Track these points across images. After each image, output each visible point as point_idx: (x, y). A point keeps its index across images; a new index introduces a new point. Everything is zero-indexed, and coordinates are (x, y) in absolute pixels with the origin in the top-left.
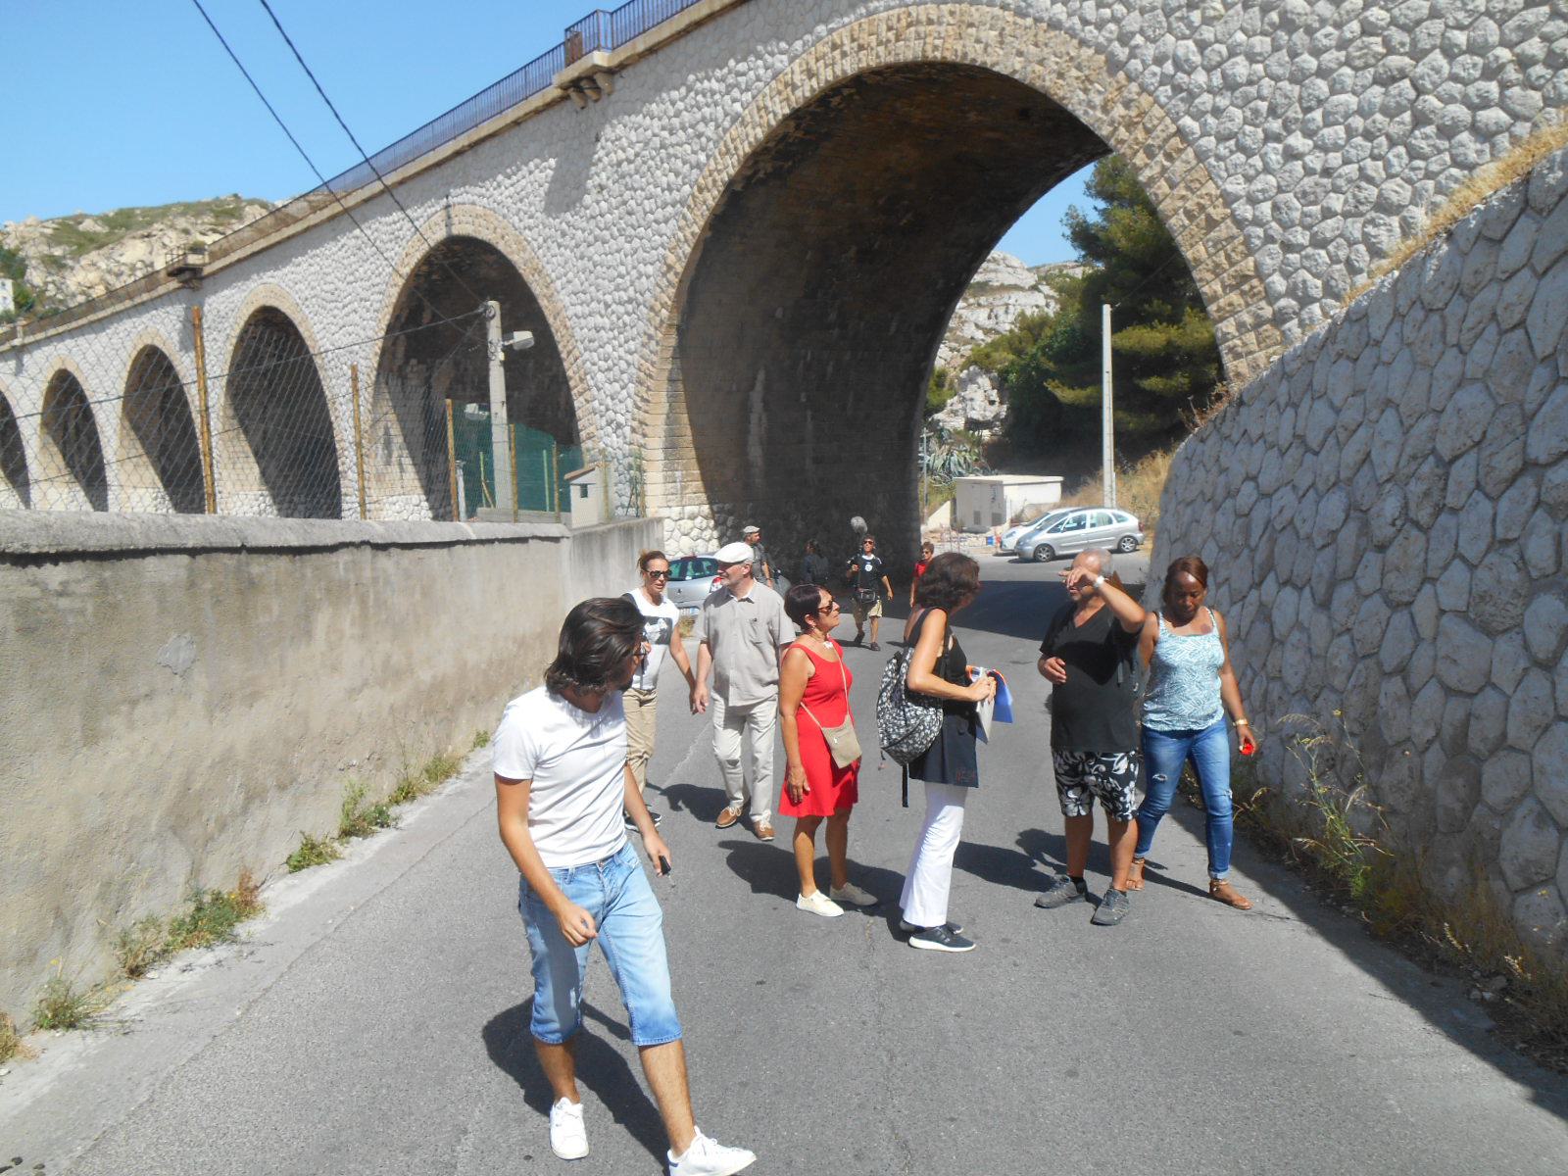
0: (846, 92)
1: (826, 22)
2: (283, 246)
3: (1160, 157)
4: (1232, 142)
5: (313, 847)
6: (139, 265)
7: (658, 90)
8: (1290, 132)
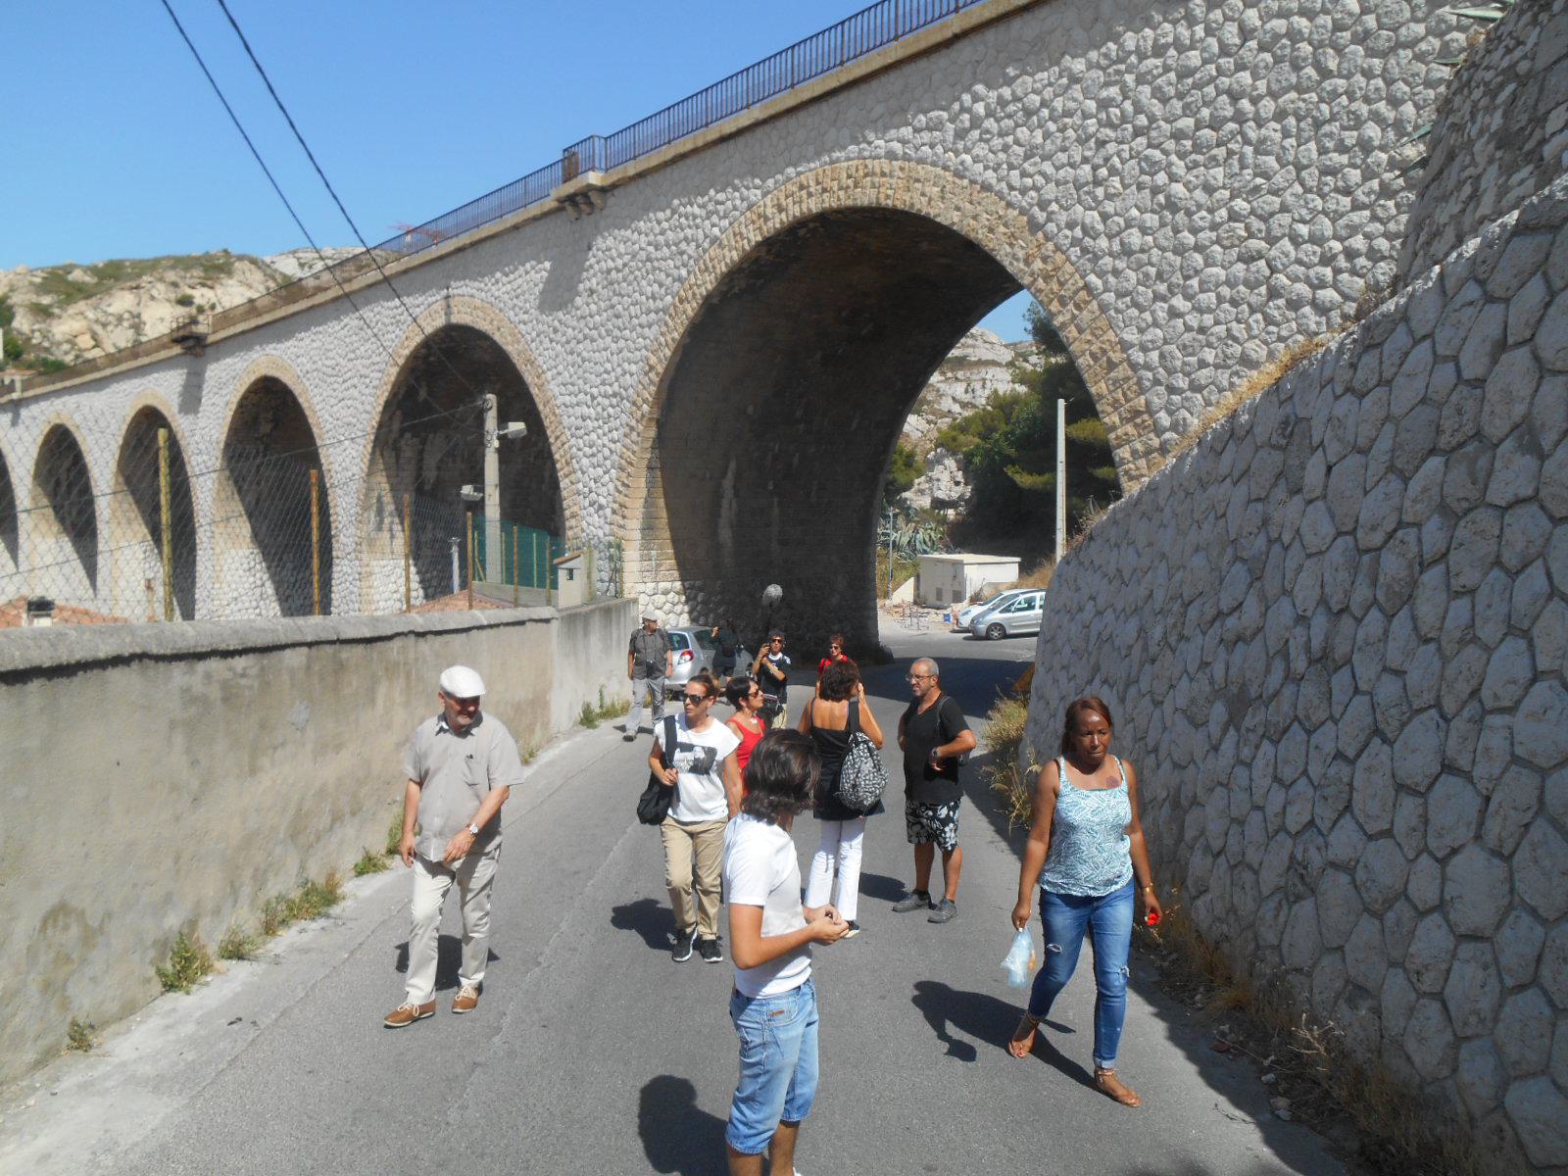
0: (811, 225)
1: (795, 166)
2: (287, 322)
3: (1071, 306)
4: (1128, 299)
5: (370, 859)
6: (126, 316)
7: (647, 209)
8: (1173, 294)
